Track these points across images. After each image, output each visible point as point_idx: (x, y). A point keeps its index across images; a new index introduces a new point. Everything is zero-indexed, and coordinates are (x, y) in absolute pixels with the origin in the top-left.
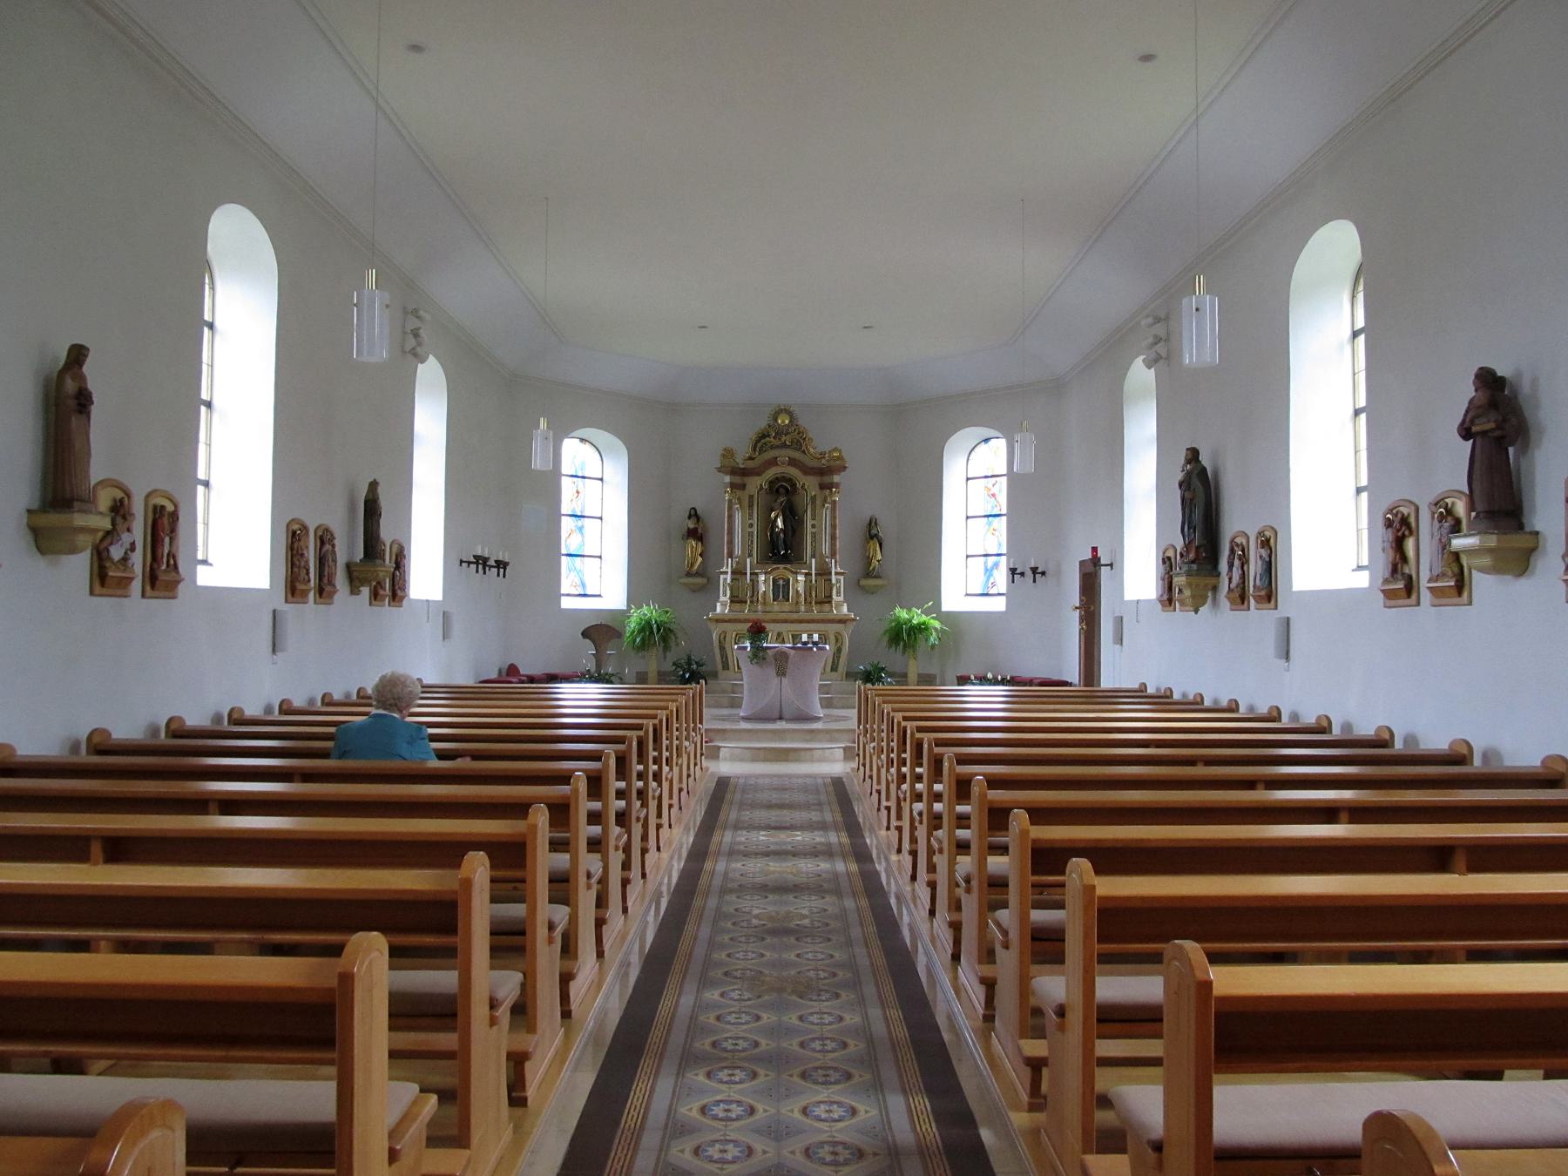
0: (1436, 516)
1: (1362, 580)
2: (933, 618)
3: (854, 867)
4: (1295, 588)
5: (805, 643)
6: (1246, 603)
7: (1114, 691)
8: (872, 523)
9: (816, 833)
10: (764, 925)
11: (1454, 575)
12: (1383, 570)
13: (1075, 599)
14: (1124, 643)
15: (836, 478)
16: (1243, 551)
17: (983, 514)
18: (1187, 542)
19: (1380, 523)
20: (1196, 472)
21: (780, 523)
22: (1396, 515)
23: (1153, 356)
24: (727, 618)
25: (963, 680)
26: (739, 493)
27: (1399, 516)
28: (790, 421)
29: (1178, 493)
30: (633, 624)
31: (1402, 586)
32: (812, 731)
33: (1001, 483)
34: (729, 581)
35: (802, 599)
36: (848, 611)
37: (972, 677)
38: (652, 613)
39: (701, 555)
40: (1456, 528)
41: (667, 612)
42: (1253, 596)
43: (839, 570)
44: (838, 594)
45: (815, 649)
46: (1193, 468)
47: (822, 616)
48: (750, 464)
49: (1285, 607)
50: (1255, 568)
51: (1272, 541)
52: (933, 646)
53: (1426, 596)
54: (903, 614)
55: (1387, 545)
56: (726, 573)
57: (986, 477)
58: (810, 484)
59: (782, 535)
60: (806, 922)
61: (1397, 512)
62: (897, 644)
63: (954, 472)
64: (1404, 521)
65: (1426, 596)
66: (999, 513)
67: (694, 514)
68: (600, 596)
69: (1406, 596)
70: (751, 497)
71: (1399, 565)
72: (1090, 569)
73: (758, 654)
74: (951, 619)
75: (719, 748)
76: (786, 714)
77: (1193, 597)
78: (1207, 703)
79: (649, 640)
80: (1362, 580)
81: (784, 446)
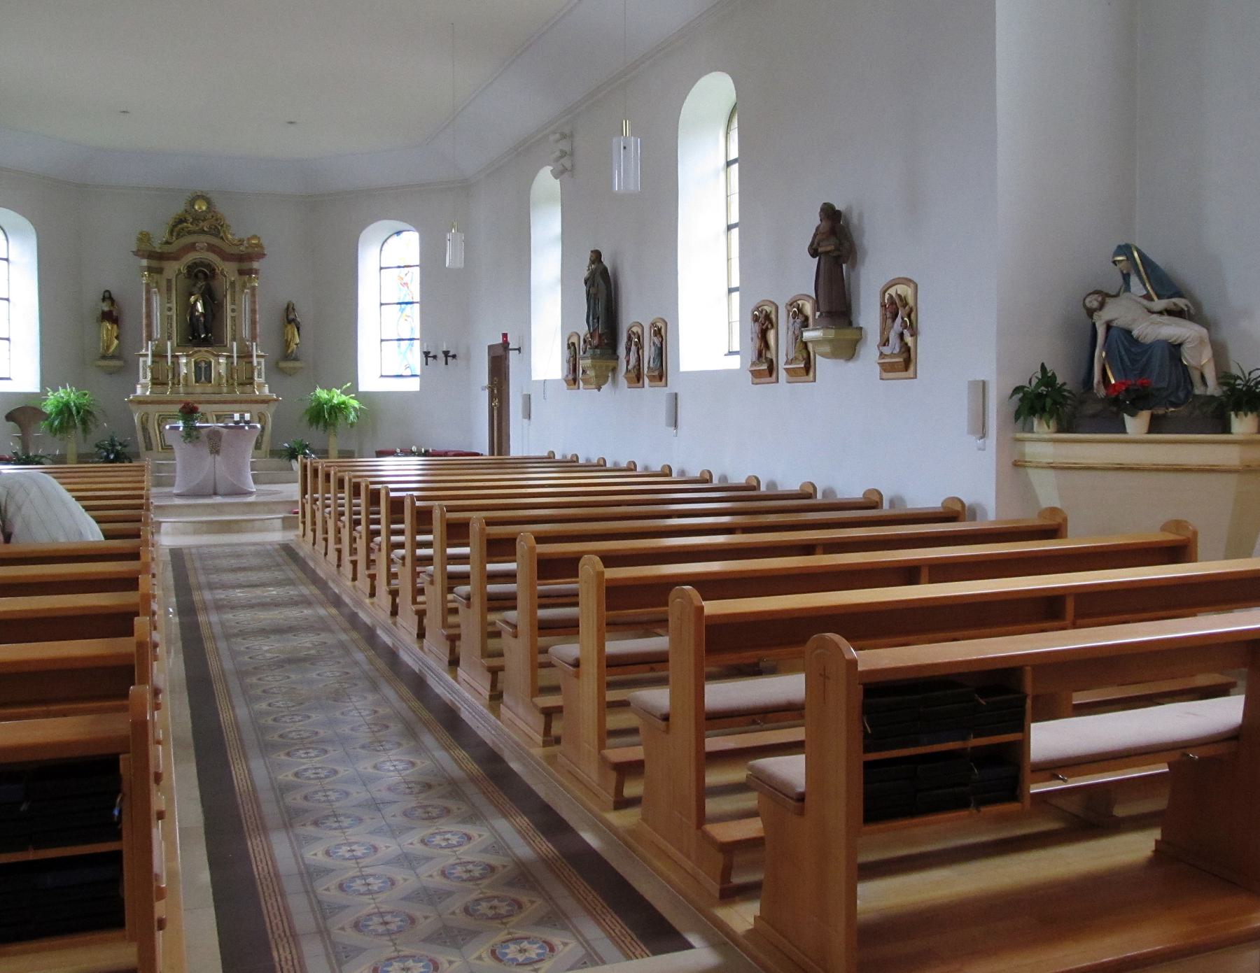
0: (791, 314)
1: (735, 363)
2: (352, 398)
3: (334, 611)
4: (682, 369)
5: (237, 423)
6: (641, 382)
7: (515, 459)
8: (289, 309)
9: (287, 588)
10: (277, 657)
11: (804, 359)
12: (751, 355)
13: (484, 379)
14: (532, 417)
15: (255, 265)
16: (639, 338)
17: (397, 302)
18: (591, 331)
19: (749, 317)
20: (599, 271)
21: (200, 307)
22: (761, 312)
23: (561, 168)
24: (149, 400)
25: (381, 454)
26: (156, 276)
27: (764, 312)
28: (208, 208)
29: (584, 288)
30: (49, 406)
31: (766, 367)
32: (250, 504)
33: (412, 273)
34: (149, 363)
35: (224, 381)
36: (270, 391)
37: (398, 450)
38: (69, 396)
39: (117, 338)
40: (805, 324)
41: (85, 394)
42: (582, 380)
43: (260, 353)
44: (259, 376)
45: (247, 428)
46: (596, 269)
47: (244, 397)
48: (167, 249)
49: (674, 384)
50: (648, 352)
51: (663, 331)
52: (352, 424)
53: (646, 381)
54: (322, 394)
55: (755, 336)
56: (146, 355)
57: (399, 267)
58: (228, 270)
59: (202, 319)
60: (312, 652)
61: (762, 310)
62: (318, 423)
63: (369, 260)
64: (768, 317)
65: (783, 375)
66: (411, 301)
67: (108, 297)
68: (9, 379)
69: (805, 374)
70: (169, 281)
71: (764, 351)
72: (500, 352)
73: (191, 434)
74: (365, 397)
75: (161, 522)
76: (221, 489)
77: (596, 376)
78: (609, 465)
79: (68, 423)
80: (735, 363)
81: (202, 232)
